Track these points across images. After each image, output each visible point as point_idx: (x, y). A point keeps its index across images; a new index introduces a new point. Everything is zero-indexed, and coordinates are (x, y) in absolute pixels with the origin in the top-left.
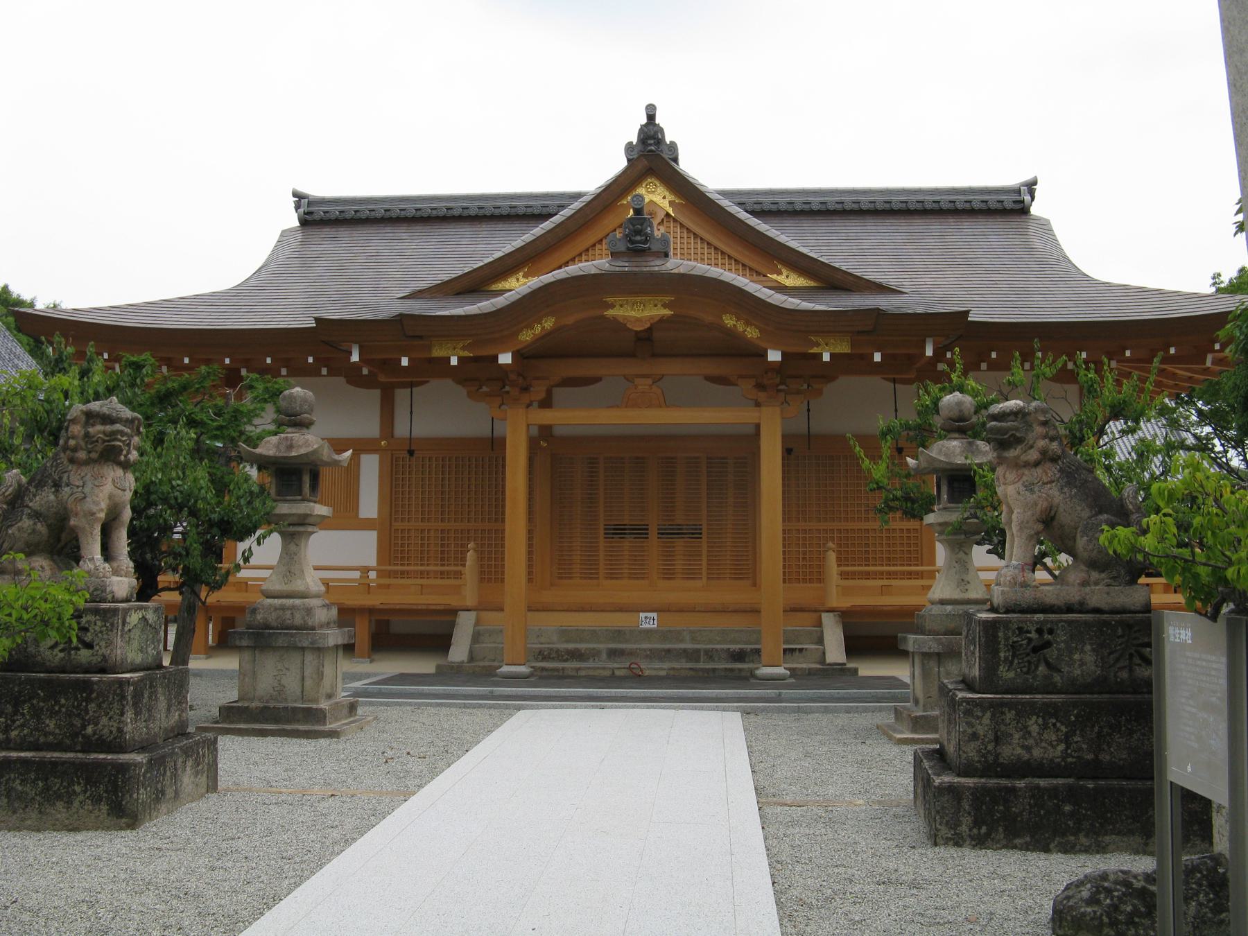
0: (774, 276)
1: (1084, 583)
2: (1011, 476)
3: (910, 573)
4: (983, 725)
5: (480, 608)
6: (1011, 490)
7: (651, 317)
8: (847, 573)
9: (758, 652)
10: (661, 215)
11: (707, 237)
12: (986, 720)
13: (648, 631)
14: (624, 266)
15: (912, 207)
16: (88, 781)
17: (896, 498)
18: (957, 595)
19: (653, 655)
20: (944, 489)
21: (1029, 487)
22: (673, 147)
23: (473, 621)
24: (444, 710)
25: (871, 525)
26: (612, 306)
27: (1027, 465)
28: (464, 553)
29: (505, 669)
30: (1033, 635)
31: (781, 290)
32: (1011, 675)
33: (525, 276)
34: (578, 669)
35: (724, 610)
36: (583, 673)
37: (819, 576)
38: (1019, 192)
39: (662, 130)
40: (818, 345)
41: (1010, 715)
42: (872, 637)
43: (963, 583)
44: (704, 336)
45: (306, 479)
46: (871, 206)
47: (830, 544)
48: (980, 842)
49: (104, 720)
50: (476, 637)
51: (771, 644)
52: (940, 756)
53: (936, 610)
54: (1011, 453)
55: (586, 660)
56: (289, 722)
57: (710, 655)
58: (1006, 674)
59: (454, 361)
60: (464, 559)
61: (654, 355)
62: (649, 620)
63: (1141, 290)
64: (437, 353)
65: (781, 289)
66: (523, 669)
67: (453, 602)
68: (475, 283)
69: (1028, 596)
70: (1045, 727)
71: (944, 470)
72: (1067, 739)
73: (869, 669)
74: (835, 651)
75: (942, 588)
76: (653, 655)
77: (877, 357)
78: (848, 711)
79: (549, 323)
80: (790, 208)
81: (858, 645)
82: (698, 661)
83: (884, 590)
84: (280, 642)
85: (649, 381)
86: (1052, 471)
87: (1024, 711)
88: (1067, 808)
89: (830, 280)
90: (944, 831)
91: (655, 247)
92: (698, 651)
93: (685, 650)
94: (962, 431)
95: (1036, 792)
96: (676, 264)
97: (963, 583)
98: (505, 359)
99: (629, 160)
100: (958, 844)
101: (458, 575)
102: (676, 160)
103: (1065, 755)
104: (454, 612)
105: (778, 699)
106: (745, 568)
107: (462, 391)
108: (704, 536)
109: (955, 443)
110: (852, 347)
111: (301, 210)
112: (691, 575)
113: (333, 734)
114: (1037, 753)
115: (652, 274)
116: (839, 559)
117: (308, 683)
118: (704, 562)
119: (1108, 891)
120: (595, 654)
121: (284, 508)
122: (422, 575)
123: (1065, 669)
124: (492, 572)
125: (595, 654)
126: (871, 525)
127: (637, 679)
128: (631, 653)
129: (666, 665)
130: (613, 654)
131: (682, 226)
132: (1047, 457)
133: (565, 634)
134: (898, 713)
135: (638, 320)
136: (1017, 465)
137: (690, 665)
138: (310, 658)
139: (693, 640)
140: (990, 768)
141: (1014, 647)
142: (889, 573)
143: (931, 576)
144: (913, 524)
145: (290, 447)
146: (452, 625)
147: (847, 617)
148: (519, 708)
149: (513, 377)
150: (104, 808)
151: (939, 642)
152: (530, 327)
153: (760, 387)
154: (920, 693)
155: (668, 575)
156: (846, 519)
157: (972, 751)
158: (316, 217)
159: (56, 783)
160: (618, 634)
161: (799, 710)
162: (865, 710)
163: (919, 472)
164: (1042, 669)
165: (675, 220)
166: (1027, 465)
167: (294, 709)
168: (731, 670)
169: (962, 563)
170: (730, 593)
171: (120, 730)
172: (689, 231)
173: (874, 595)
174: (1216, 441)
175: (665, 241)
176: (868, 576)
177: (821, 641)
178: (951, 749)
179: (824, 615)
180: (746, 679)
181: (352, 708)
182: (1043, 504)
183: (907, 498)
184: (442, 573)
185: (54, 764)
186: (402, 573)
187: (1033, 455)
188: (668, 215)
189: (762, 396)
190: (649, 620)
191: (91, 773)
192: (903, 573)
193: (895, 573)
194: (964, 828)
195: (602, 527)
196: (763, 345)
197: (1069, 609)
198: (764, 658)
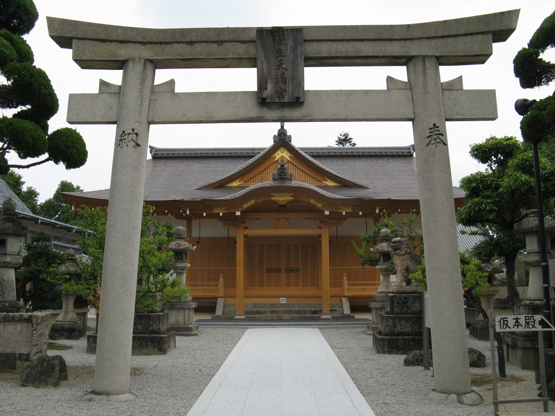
0: (325, 182)
1: (417, 286)
2: (398, 258)
3: (372, 284)
4: (390, 323)
5: (225, 297)
6: (397, 262)
8: (350, 284)
9: (321, 311)
10: (286, 161)
11: (302, 169)
12: (391, 322)
13: (283, 304)
14: (277, 184)
15: (372, 154)
16: (152, 342)
17: (367, 260)
18: (385, 290)
19: (285, 312)
20: (382, 258)
21: (402, 261)
22: (290, 137)
23: (223, 302)
24: (224, 329)
25: (358, 267)
26: (274, 196)
27: (402, 255)
28: (219, 278)
29: (237, 317)
30: (403, 300)
31: (327, 191)
32: (398, 310)
34: (260, 317)
35: (298, 297)
36: (262, 318)
37: (341, 285)
38: (409, 149)
39: (286, 131)
40: (341, 209)
41: (397, 320)
42: (359, 306)
43: (388, 287)
44: (303, 205)
45: (184, 255)
46: (357, 154)
47: (345, 274)
48: (390, 353)
49: (154, 326)
50: (224, 307)
51: (326, 308)
52: (380, 333)
53: (379, 295)
54: (397, 252)
55: (263, 314)
56: (181, 331)
57: (305, 312)
58: (396, 310)
59: (221, 214)
60: (219, 280)
61: (287, 211)
62: (283, 301)
64: (216, 211)
65: (326, 188)
66: (243, 317)
67: (215, 294)
68: (221, 185)
69: (402, 289)
70: (406, 323)
71: (382, 252)
72: (412, 326)
73: (357, 316)
74: (347, 310)
75: (381, 288)
76: (285, 312)
77: (361, 213)
78: (352, 328)
79: (253, 202)
80: (329, 154)
81: (355, 309)
82: (300, 314)
83: (363, 290)
84: (178, 306)
85: (284, 220)
86: (407, 257)
87: (401, 319)
88: (412, 343)
89: (344, 184)
90: (381, 350)
91: (288, 177)
92: (300, 311)
93: (296, 311)
94: (387, 240)
95: (404, 340)
96: (295, 183)
97: (388, 287)
98: (238, 213)
99: (274, 142)
100: (384, 353)
101: (217, 285)
102: (291, 142)
103: (411, 330)
104: (216, 298)
105: (330, 325)
106: (315, 282)
107: (221, 223)
108: (301, 271)
109: (385, 244)
110: (353, 209)
111: (153, 153)
112: (296, 285)
113: (196, 335)
114: (404, 330)
115: (287, 186)
116: (347, 279)
117: (186, 319)
118: (301, 279)
119: (416, 356)
120: (266, 312)
121: (178, 265)
122: (202, 285)
123: (412, 308)
124: (231, 283)
125: (266, 312)
126: (358, 267)
127: (280, 319)
128: (278, 312)
129: (290, 316)
130: (272, 312)
131: (293, 164)
132: (406, 253)
133: (255, 305)
134: (368, 327)
135: (282, 201)
136: (399, 255)
137: (298, 315)
138: (186, 311)
139: (298, 307)
140: (392, 334)
141: (398, 303)
142: (365, 284)
143: (379, 284)
144: (373, 268)
145: (180, 246)
146: (216, 302)
147: (350, 299)
148: (249, 328)
149: (239, 219)
150: (157, 349)
151: (380, 304)
153: (322, 222)
154: (375, 320)
155: (288, 285)
156: (350, 265)
157: (387, 330)
158: (159, 156)
159: (143, 343)
160: (273, 305)
161: (337, 328)
162: (358, 327)
163: (374, 252)
164: (406, 308)
165: (291, 162)
166: (402, 255)
167: (182, 328)
168: (312, 317)
169: (388, 281)
170: (313, 291)
171: (159, 328)
172: (295, 166)
173: (358, 291)
174: (490, 231)
175: (291, 175)
176: (357, 285)
177: (342, 307)
178: (382, 330)
179: (343, 298)
180: (319, 319)
181: (198, 327)
183: (370, 260)
184: (202, 285)
185: (142, 337)
186: (195, 285)
187: (403, 252)
188: (288, 161)
189: (322, 225)
190: (283, 301)
191: (153, 340)
192: (369, 284)
193: (367, 284)
194: (386, 349)
195: (265, 268)
196: (324, 209)
197: (413, 293)
198: (324, 313)
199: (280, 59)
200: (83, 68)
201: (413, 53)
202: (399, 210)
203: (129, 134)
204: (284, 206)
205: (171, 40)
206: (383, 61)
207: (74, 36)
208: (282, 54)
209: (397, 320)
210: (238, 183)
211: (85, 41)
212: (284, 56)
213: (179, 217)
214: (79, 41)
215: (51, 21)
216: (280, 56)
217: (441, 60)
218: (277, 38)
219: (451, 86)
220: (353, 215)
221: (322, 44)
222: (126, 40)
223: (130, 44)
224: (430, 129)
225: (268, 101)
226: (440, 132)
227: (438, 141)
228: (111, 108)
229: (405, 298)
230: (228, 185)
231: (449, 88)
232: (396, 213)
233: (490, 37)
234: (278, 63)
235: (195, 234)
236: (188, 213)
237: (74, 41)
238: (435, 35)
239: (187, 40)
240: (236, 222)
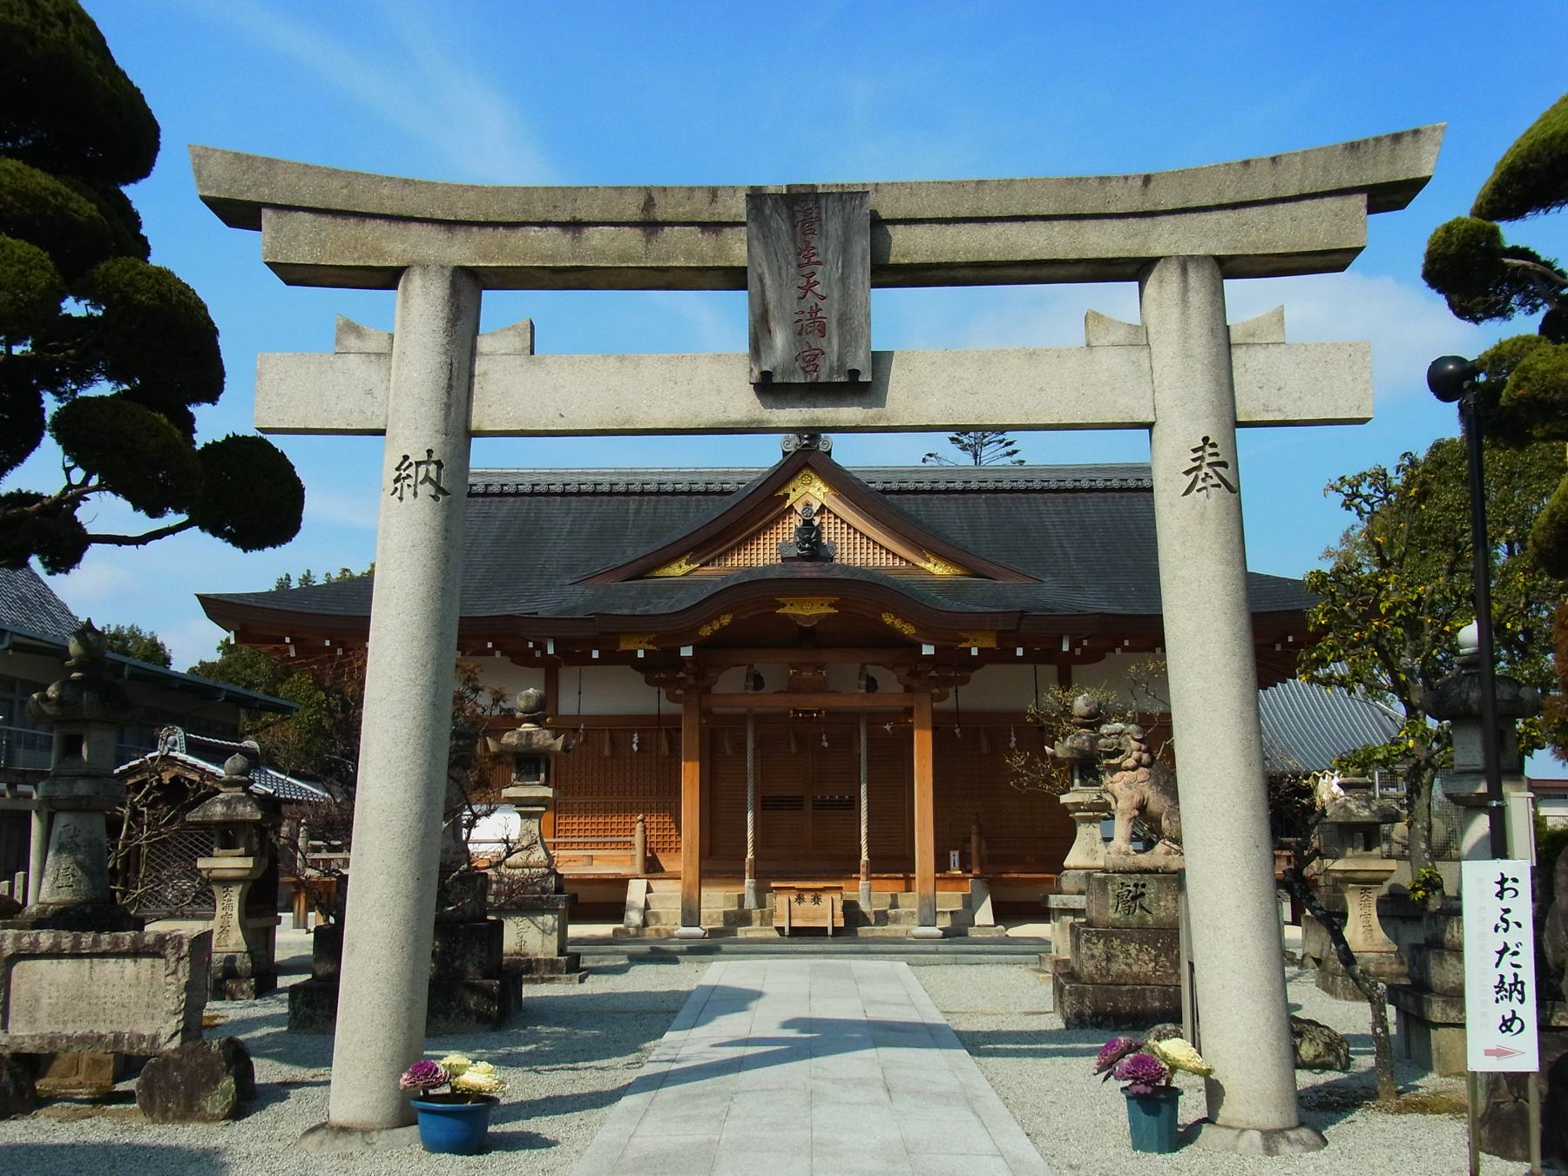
1: (1168, 853)
7: (818, 616)
12: (1100, 945)
21: (1128, 785)
26: (784, 606)
33: (688, 563)
40: (966, 640)
41: (1116, 943)
59: (641, 654)
63: (734, 989)
64: (625, 646)
70: (1140, 950)
72: (1156, 960)
92: (877, 923)
98: (687, 652)
99: (785, 454)
107: (640, 677)
110: (999, 641)
114: (1135, 968)
149: (689, 665)
152: (723, 628)
182: (1137, 798)
187: (1130, 762)
199: (807, 271)
200: (288, 283)
201: (1157, 251)
202: (1126, 643)
203: (418, 464)
204: (811, 631)
205: (522, 218)
206: (1078, 270)
207: (266, 199)
208: (814, 259)
209: (1116, 943)
210: (686, 568)
211: (295, 215)
212: (819, 263)
213: (523, 659)
214: (280, 214)
215: (201, 158)
216: (809, 263)
217: (1228, 265)
218: (800, 217)
219: (1253, 335)
220: (1001, 655)
221: (918, 230)
222: (405, 213)
223: (415, 227)
224: (1195, 451)
225: (777, 379)
226: (1220, 459)
227: (1216, 480)
228: (370, 392)
229: (1136, 885)
230: (657, 574)
231: (1250, 340)
232: (1118, 651)
233: (1361, 200)
234: (803, 282)
235: (568, 704)
236: (551, 651)
237: (267, 214)
238: (1218, 201)
239: (565, 217)
240: (682, 675)
